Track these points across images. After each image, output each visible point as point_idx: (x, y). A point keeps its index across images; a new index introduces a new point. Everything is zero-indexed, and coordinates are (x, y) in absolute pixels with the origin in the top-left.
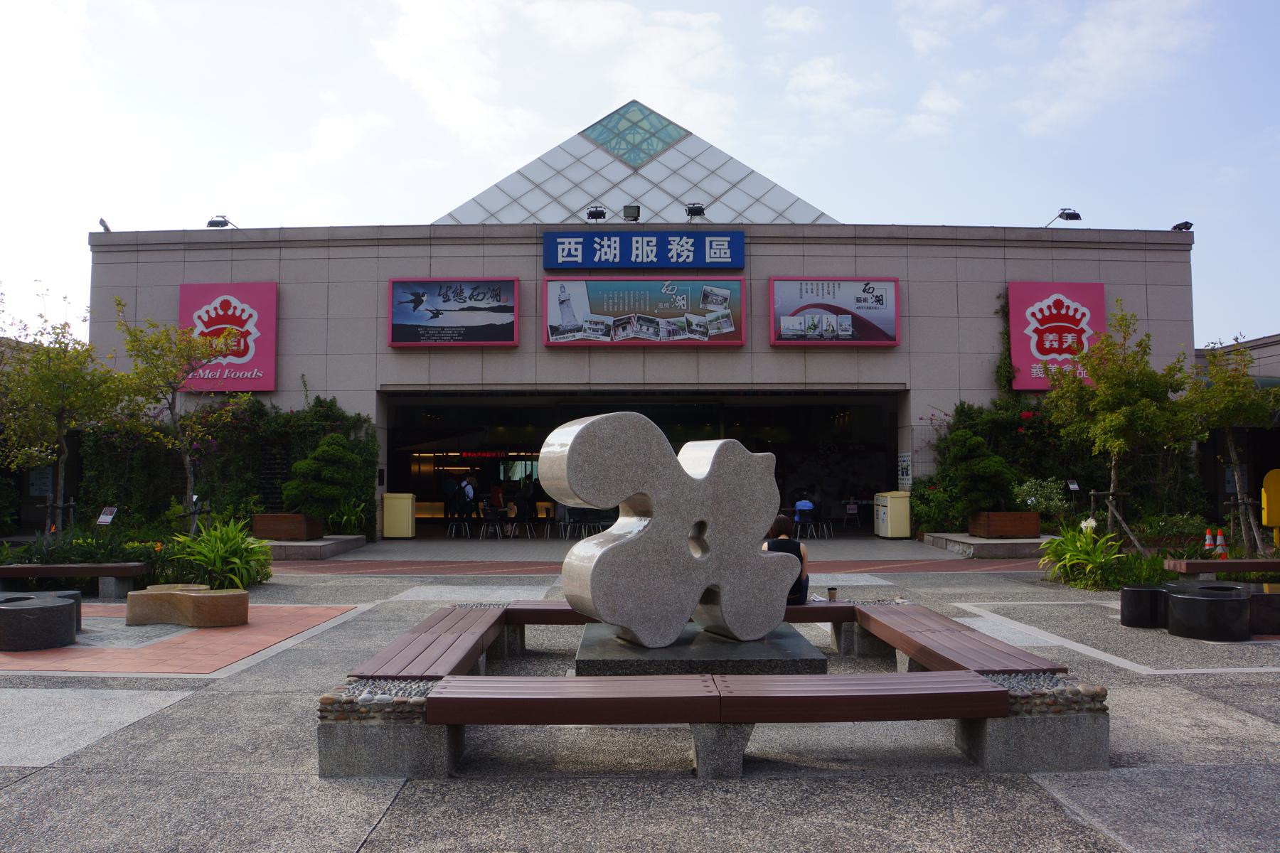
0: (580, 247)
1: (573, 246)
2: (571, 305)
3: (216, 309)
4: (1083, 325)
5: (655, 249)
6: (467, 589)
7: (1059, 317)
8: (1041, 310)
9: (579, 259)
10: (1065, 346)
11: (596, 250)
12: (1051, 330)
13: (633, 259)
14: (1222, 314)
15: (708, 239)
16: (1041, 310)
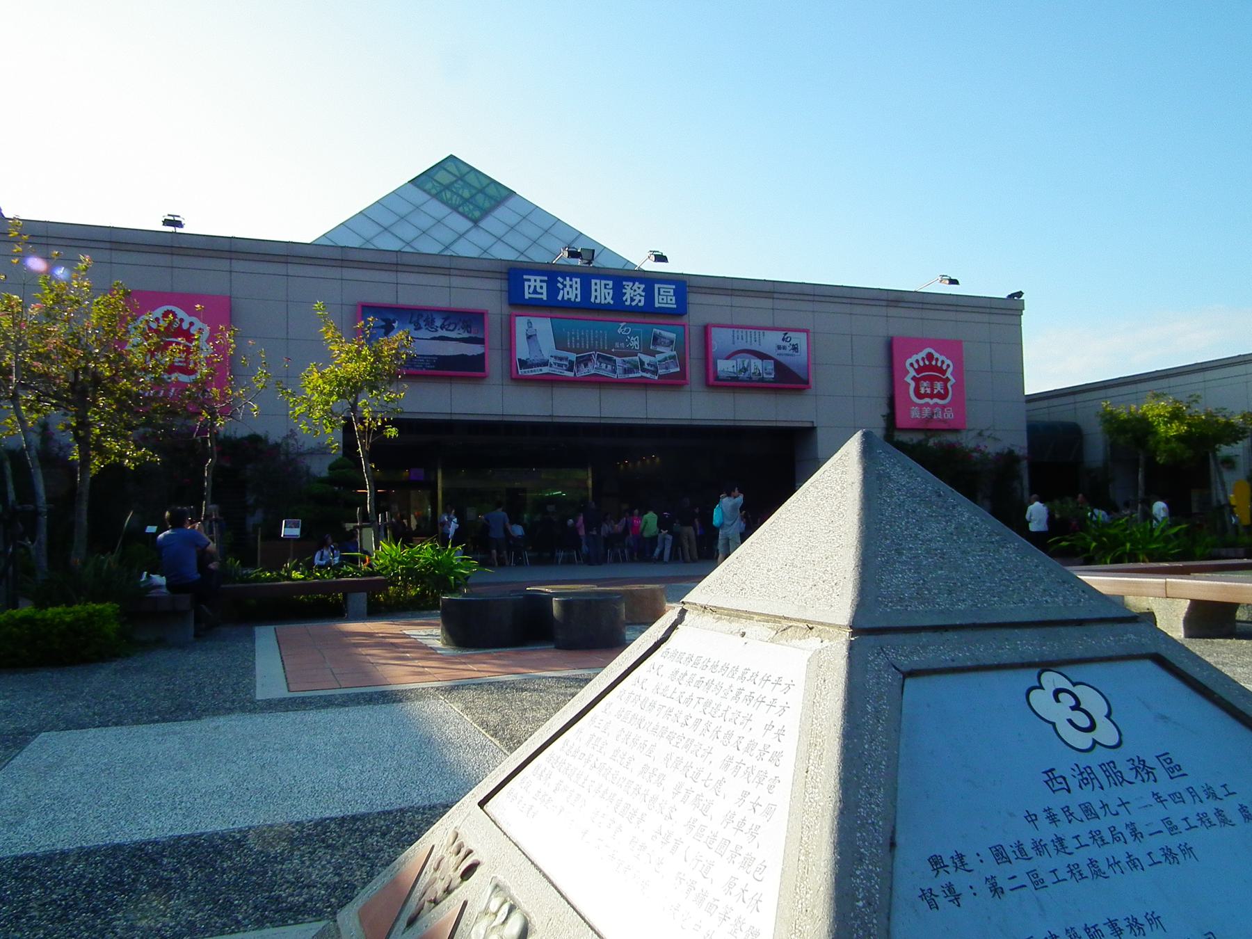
0: (544, 285)
1: (538, 284)
2: (537, 337)
4: (948, 374)
8: (917, 361)
9: (544, 297)
12: (924, 379)
15: (656, 286)
16: (917, 361)
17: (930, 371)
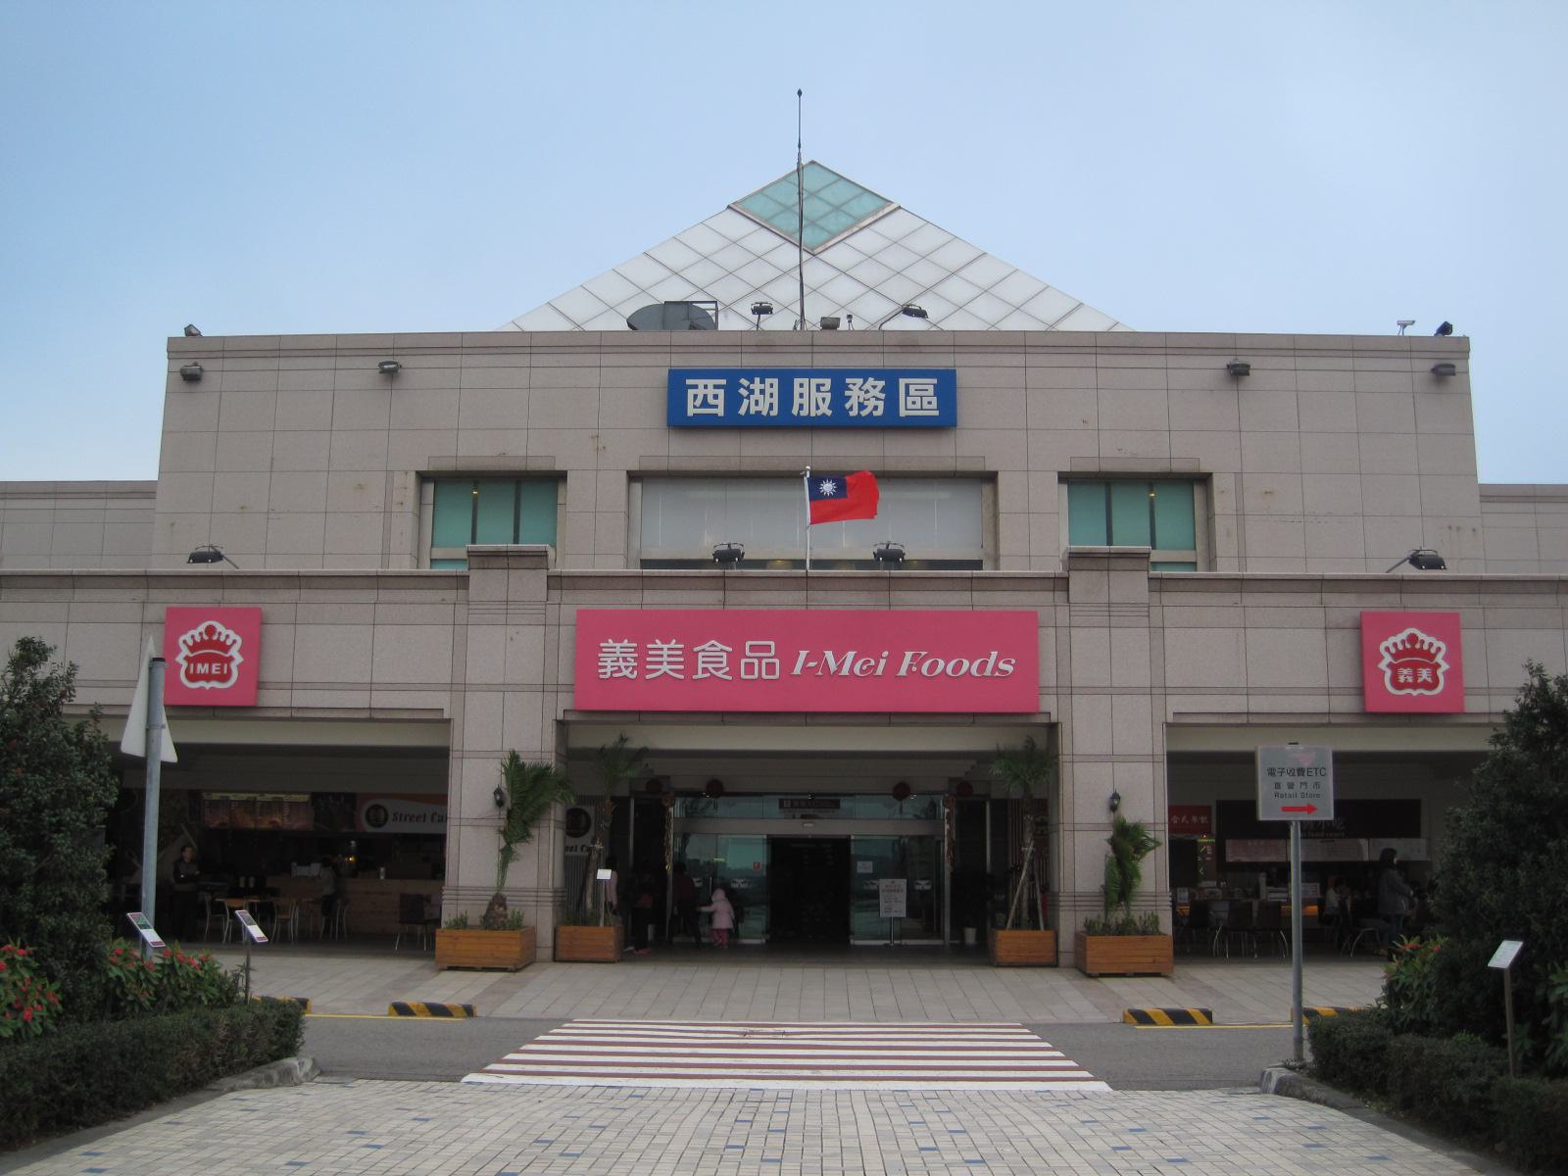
0: (721, 393)
1: (711, 392)
3: (201, 634)
4: (1439, 659)
5: (828, 396)
6: (156, 821)
7: (1412, 652)
8: (1395, 645)
9: (720, 411)
10: (1420, 680)
11: (741, 398)
12: (1405, 665)
13: (795, 411)
14: (1511, 441)
15: (902, 382)
16: (1395, 645)
17: (1413, 656)
